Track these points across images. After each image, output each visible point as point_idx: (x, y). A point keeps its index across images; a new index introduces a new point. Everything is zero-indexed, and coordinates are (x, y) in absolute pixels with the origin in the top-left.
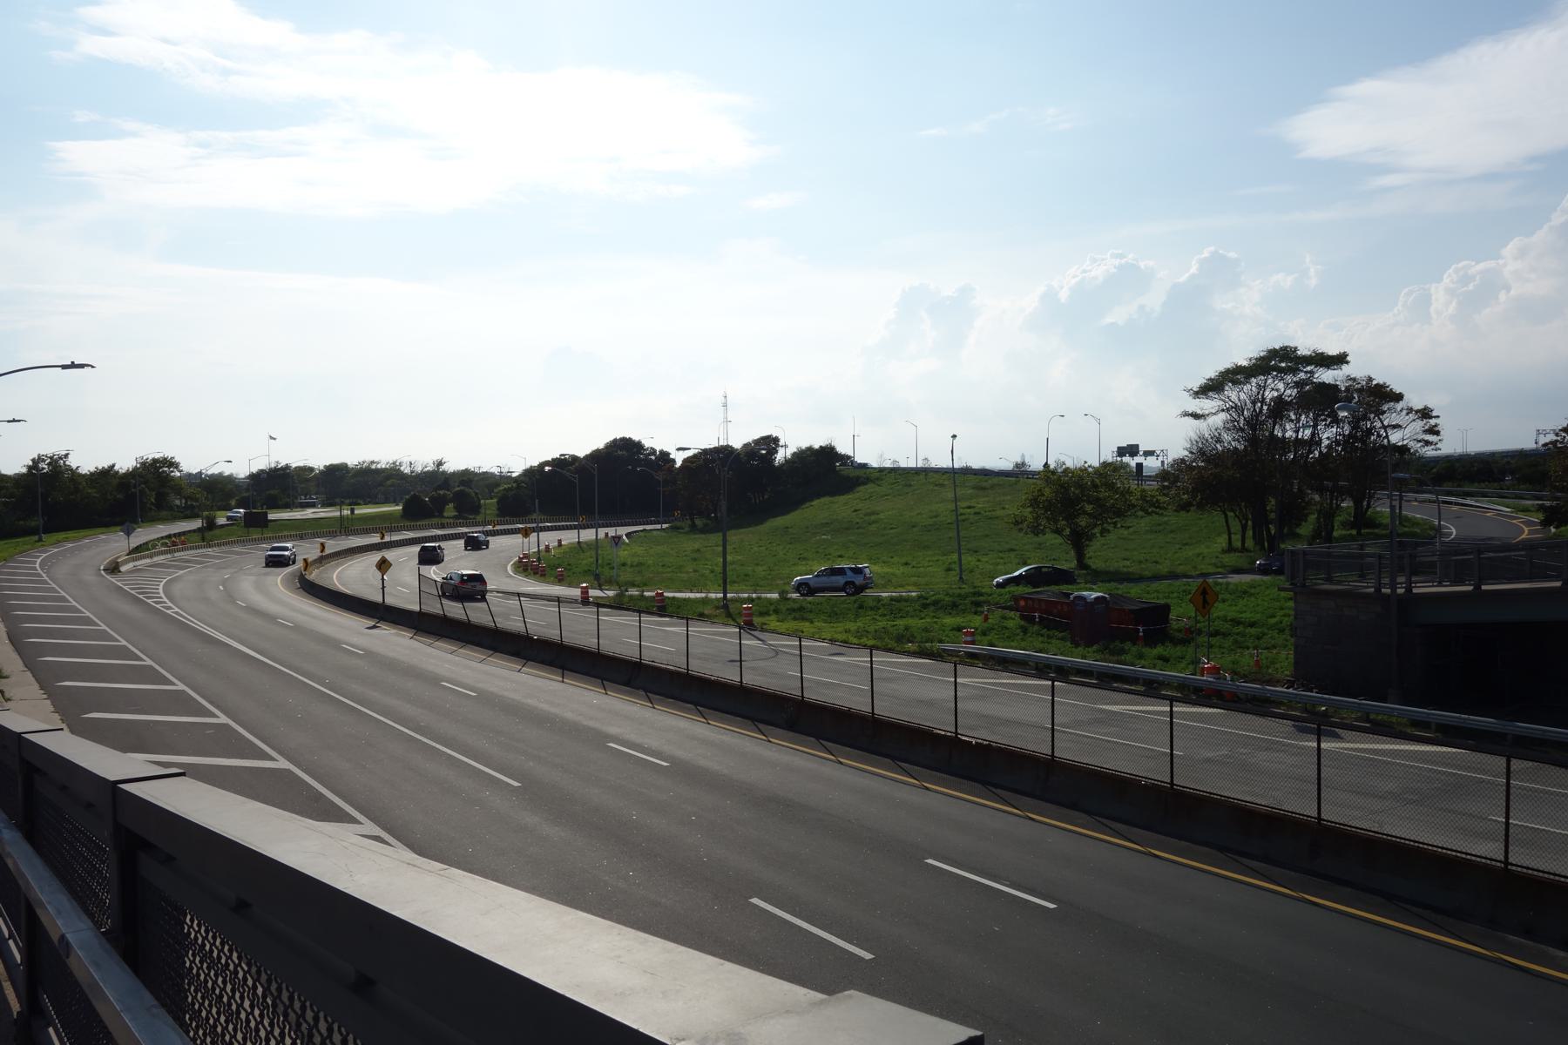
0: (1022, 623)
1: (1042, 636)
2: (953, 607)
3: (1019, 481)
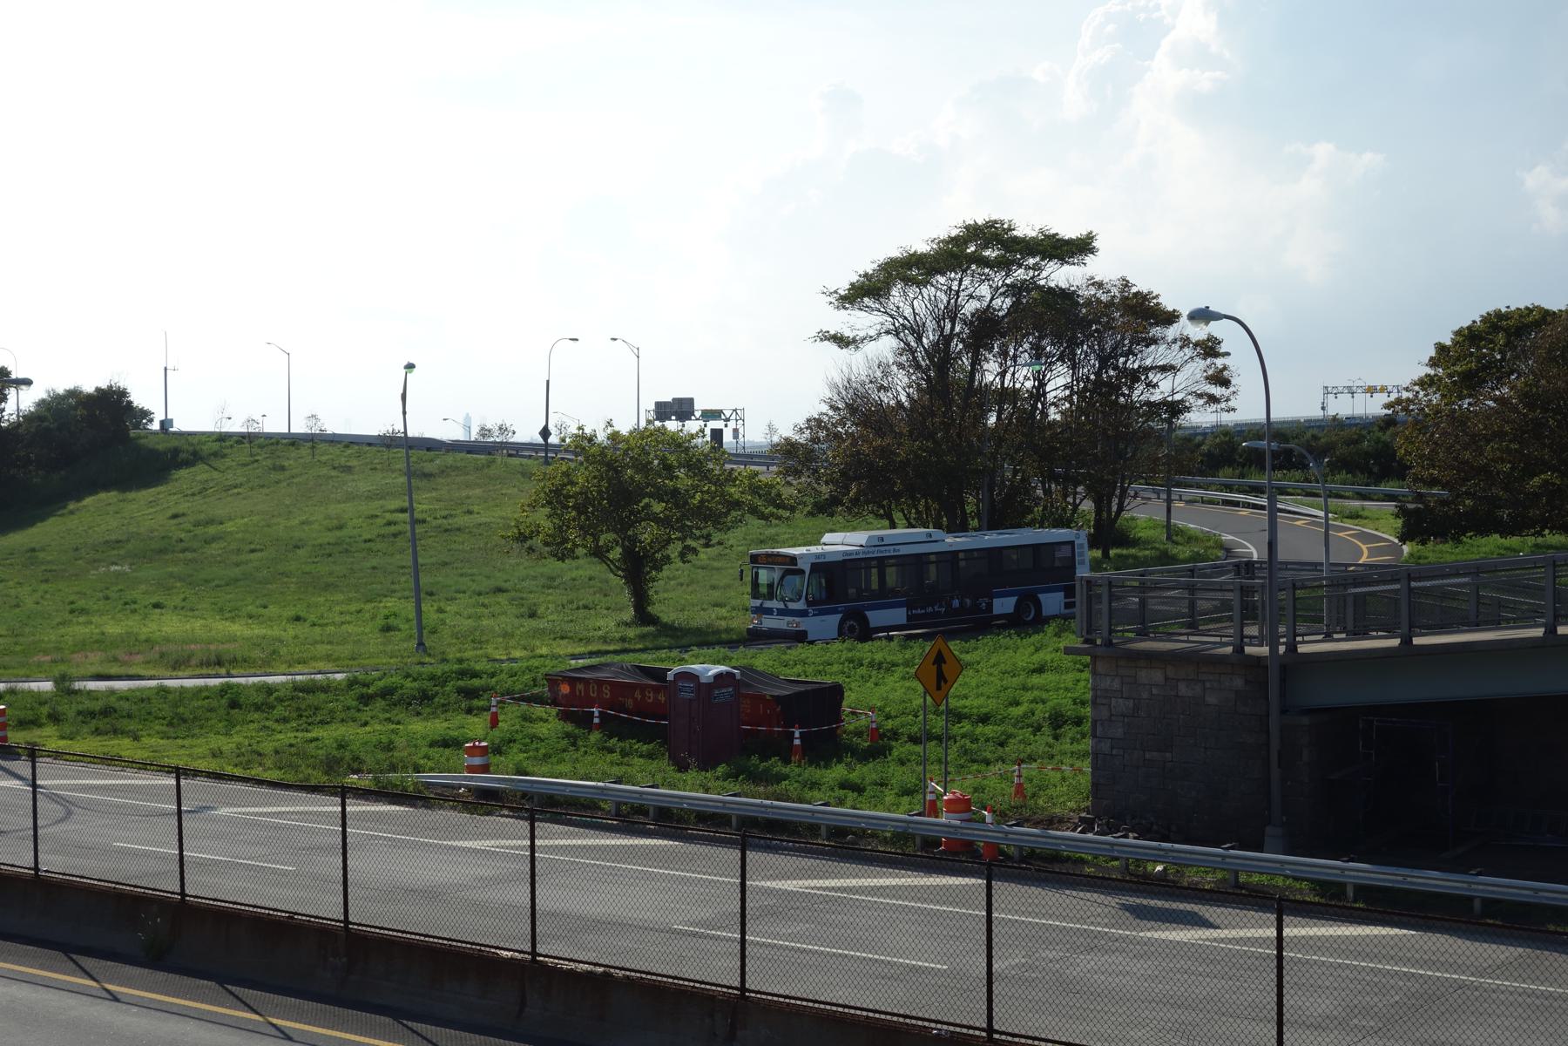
0: (569, 727)
1: (611, 751)
2: (423, 701)
3: (494, 461)
